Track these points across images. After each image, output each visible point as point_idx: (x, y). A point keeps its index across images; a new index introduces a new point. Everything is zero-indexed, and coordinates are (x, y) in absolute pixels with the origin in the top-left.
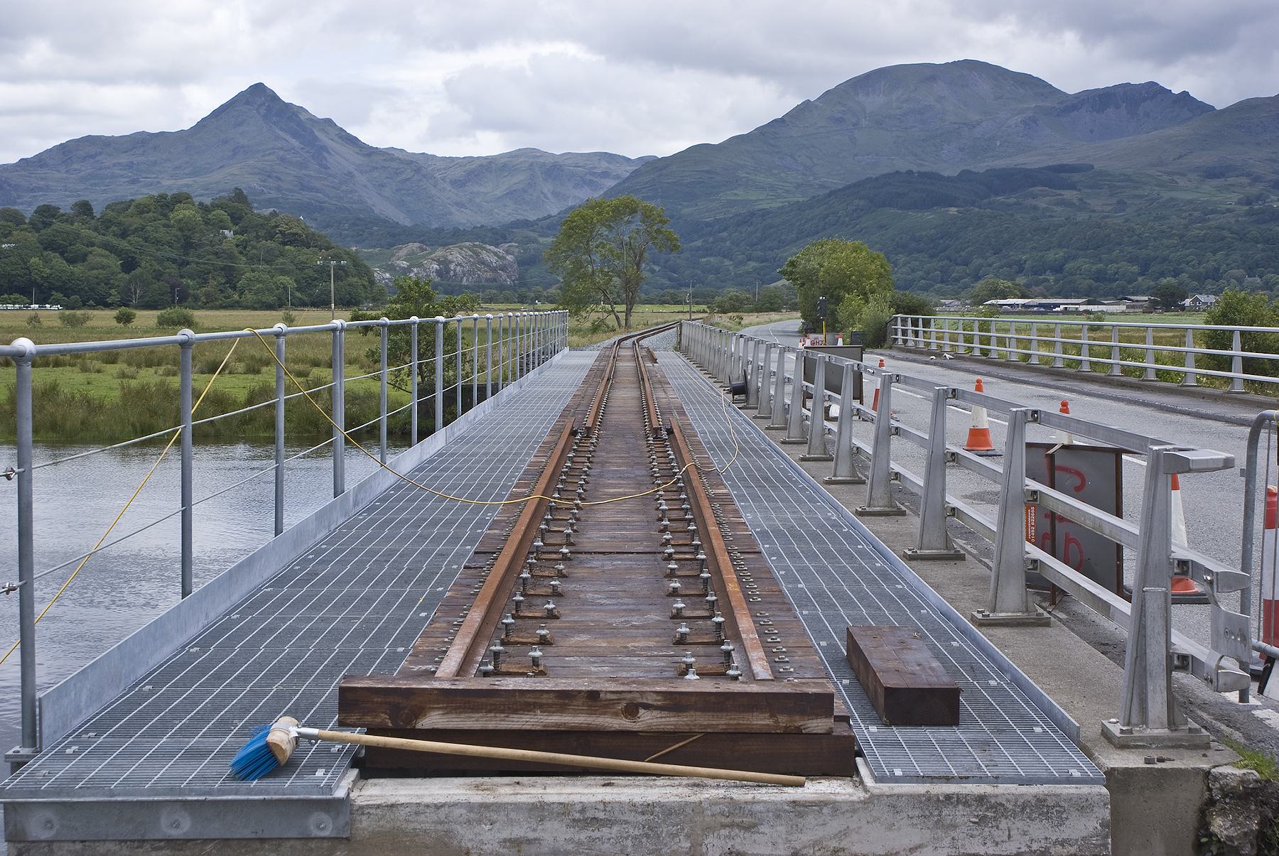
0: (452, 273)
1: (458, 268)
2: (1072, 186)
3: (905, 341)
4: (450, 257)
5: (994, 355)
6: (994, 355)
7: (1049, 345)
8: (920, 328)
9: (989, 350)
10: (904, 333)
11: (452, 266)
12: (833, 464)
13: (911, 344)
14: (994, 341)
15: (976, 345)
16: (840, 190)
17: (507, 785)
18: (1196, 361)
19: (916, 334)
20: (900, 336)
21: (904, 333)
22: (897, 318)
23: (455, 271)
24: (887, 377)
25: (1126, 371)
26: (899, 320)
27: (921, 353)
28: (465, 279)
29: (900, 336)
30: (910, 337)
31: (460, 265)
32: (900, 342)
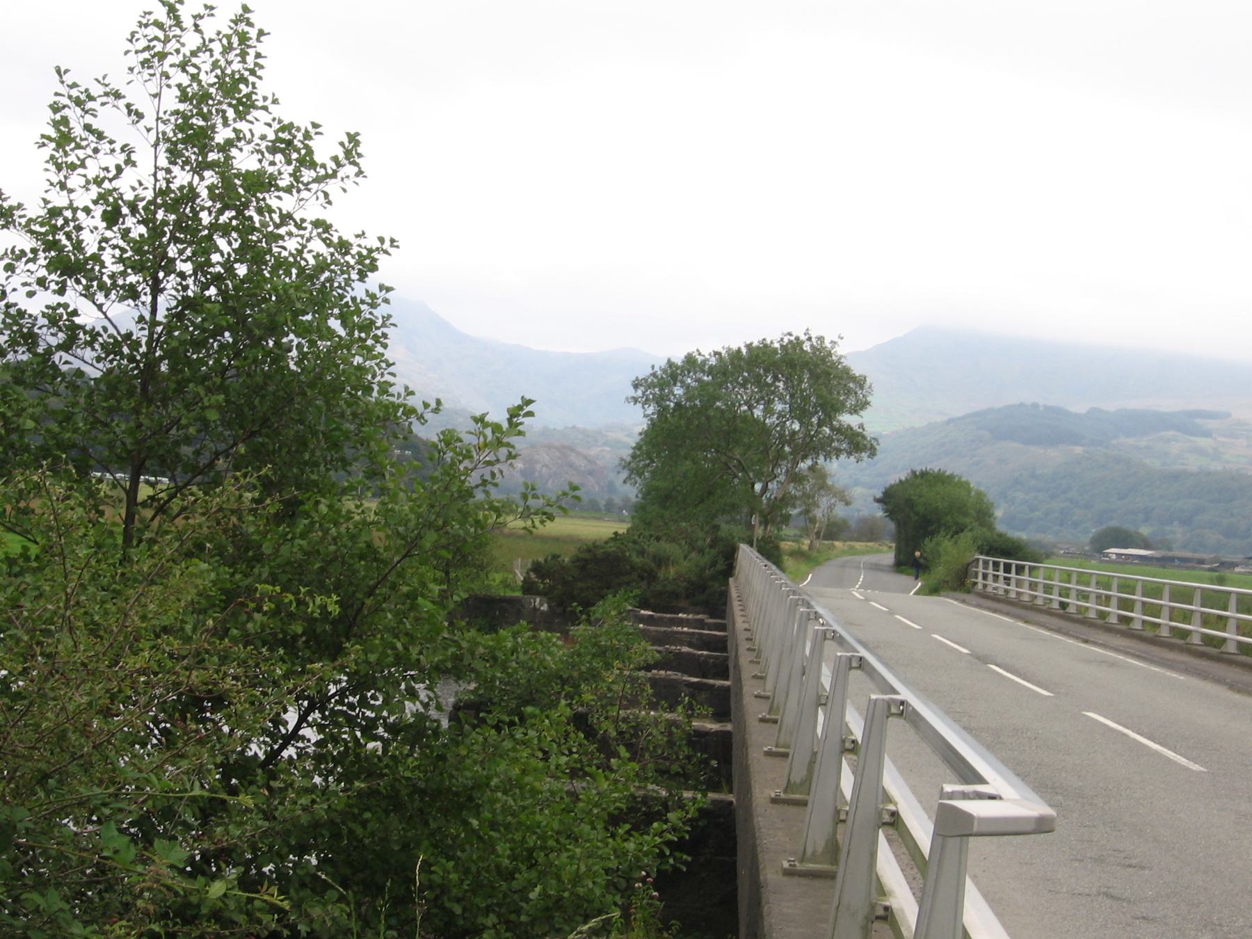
0: (537, 474)
1: (544, 470)
2: (1207, 434)
3: (985, 586)
4: (536, 457)
5: (1072, 609)
6: (1072, 609)
7: (1084, 596)
8: (1013, 575)
9: (1068, 604)
10: (985, 577)
11: (538, 467)
12: (777, 726)
13: (989, 589)
14: (1073, 594)
15: (1055, 597)
16: (959, 418)
17: (960, 854)
18: (1238, 628)
19: (996, 578)
20: (980, 579)
21: (985, 577)
22: (978, 560)
23: (540, 472)
24: (805, 615)
25: (1208, 640)
26: (981, 562)
27: (1025, 607)
28: (550, 481)
29: (980, 579)
30: (990, 581)
31: (546, 466)
32: (980, 586)
